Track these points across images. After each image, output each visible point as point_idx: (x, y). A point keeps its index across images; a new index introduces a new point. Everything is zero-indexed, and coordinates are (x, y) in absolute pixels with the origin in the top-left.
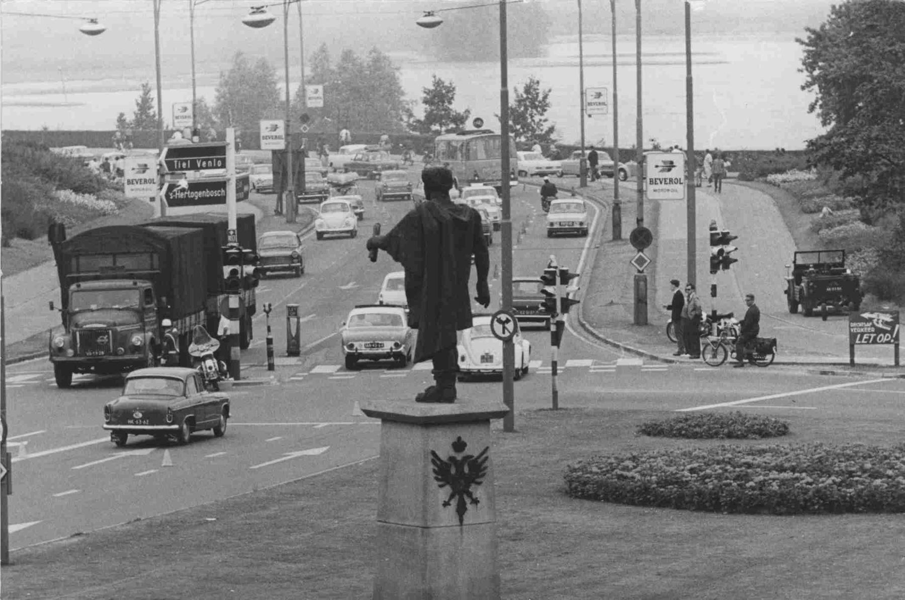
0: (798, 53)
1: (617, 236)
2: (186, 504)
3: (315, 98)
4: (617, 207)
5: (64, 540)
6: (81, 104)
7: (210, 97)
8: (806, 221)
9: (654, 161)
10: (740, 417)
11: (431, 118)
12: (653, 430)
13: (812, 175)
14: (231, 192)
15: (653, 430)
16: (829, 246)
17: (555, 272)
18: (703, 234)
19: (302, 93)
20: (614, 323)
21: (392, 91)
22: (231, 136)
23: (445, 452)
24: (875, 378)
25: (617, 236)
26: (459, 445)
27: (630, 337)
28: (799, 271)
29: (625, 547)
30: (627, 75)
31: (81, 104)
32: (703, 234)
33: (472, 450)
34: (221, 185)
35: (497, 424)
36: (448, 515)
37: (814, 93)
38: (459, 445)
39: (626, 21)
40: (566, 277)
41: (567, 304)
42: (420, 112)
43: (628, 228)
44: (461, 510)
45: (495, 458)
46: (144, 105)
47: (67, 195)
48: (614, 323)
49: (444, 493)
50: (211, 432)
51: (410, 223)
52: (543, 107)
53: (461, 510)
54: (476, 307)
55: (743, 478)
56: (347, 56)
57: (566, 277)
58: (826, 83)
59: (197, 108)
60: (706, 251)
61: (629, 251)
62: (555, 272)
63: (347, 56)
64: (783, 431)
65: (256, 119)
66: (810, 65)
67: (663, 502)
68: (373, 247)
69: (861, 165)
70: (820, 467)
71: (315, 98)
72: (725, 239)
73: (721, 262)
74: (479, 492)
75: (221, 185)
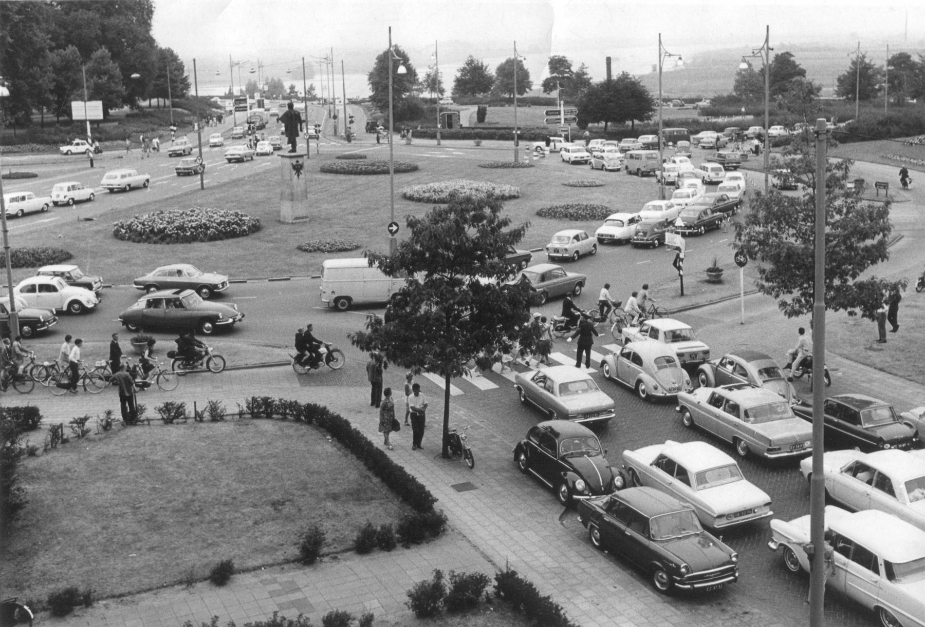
0: (366, 77)
1: (330, 117)
2: (240, 176)
3: (266, 88)
4: (330, 111)
5: (215, 184)
6: (565, 185)
7: (244, 88)
8: (369, 113)
9: (337, 102)
10: (356, 155)
11: (291, 93)
12: (338, 158)
13: (370, 103)
14: (248, 108)
15: (338, 158)
16: (374, 118)
17: (556, 105)
18: (348, 116)
19: (263, 88)
20: (330, 135)
21: (282, 87)
22: (248, 96)
23: (295, 163)
24: (384, 146)
25: (330, 117)
26: (297, 162)
27: (333, 138)
28: (368, 124)
29: (333, 182)
30: (331, 83)
31: (565, 185)
32: (348, 116)
33: (300, 162)
34: (246, 107)
35: (305, 157)
36: (296, 177)
37: (371, 86)
38: (297, 162)
39: (330, 71)
40: (319, 126)
41: (319, 131)
42: (288, 91)
43: (332, 115)
44: (298, 176)
45: (306, 164)
46: (230, 90)
47: (214, 110)
48: (330, 135)
49: (294, 172)
50: (249, 158)
51: (286, 115)
52: (314, 90)
53: (298, 176)
54: (300, 133)
55: (357, 167)
56: (272, 79)
57: (319, 126)
58: (372, 83)
59: (241, 91)
60: (348, 120)
61: (332, 120)
62: (556, 105)
63: (272, 79)
64: (365, 157)
65: (253, 93)
66: (369, 79)
67: (341, 173)
68: (278, 120)
69: (380, 101)
70: (373, 165)
71: (266, 88)
72: (351, 117)
73: (351, 122)
74: (302, 171)
75: (246, 107)
